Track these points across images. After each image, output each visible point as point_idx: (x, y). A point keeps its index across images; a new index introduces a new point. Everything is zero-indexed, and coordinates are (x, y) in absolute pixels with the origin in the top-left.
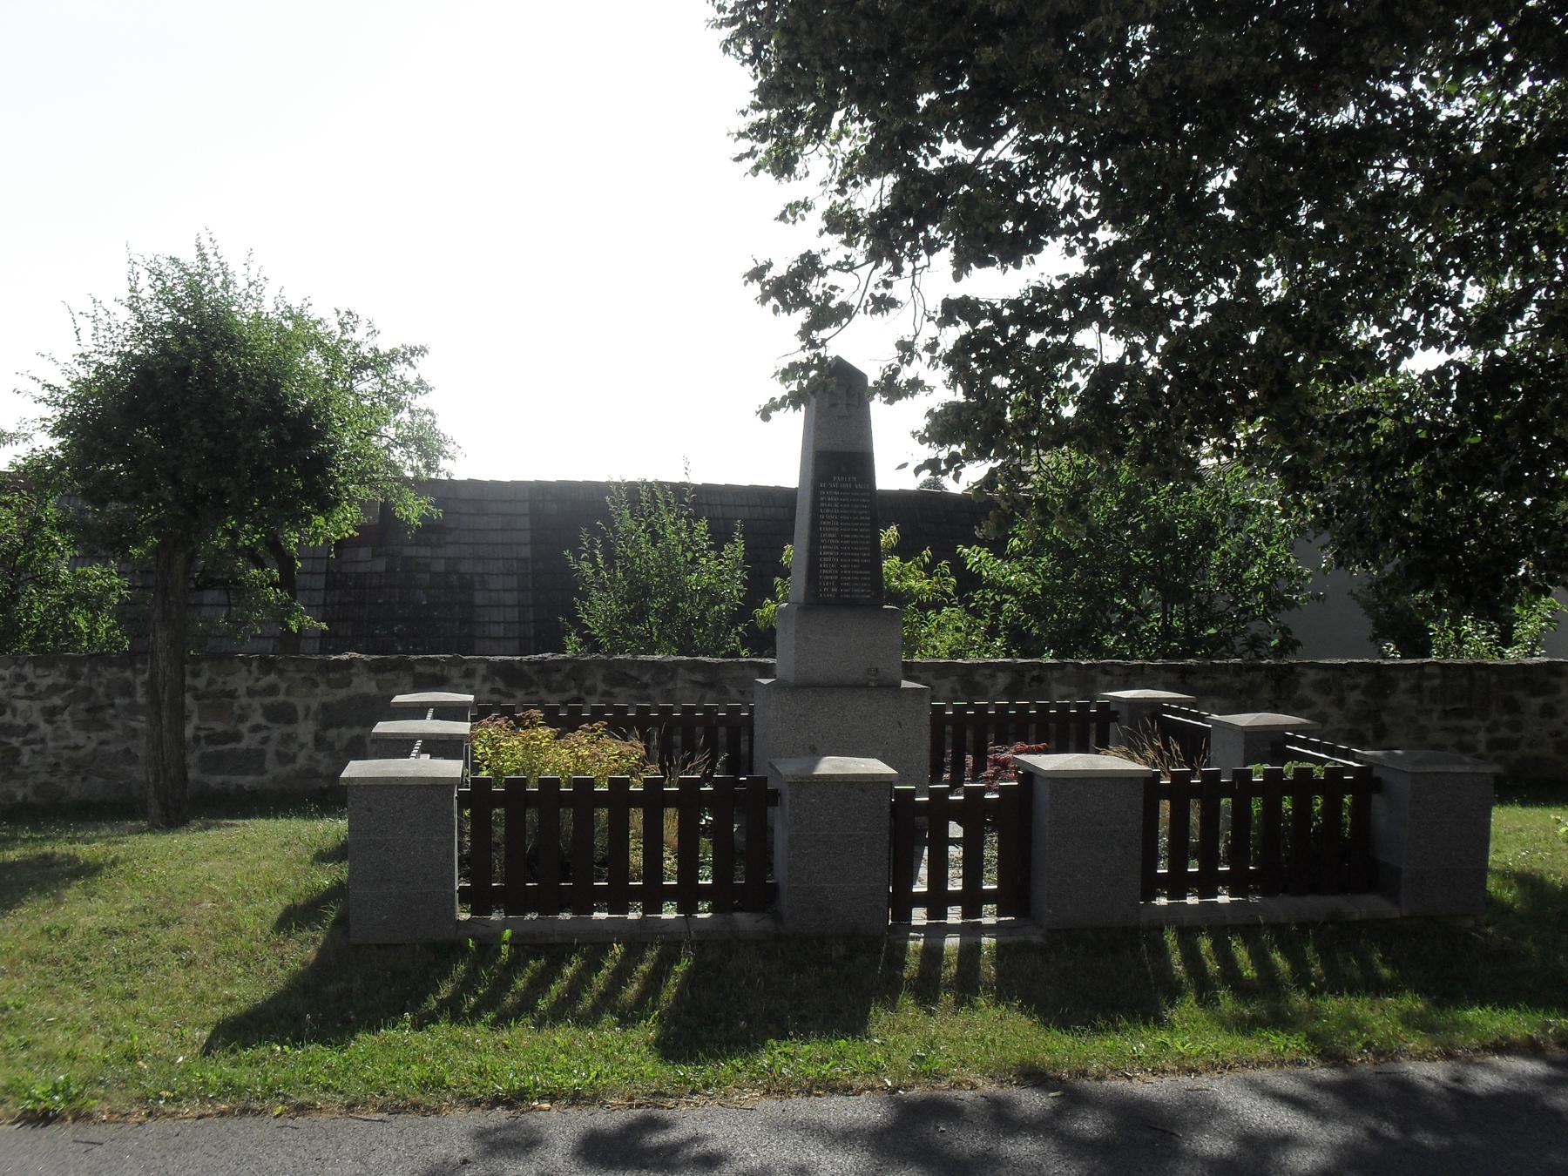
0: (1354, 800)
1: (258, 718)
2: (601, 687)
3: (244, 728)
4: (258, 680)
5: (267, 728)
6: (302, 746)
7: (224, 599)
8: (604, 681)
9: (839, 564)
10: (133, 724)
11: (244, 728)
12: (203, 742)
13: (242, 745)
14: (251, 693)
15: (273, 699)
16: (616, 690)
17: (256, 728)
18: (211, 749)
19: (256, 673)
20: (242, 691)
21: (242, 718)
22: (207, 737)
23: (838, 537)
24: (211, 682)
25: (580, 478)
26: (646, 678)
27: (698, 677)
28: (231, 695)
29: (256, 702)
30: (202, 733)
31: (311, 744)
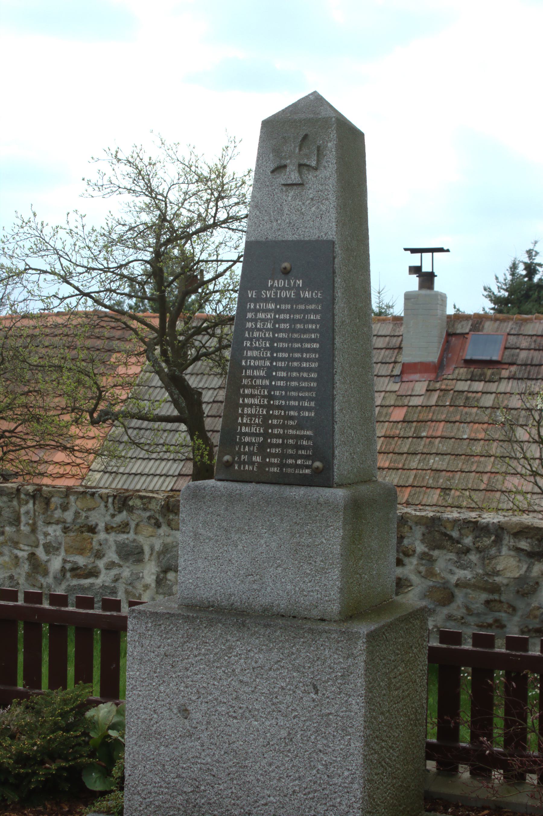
0: (463, 666)
1: (112, 555)
2: (420, 548)
3: (101, 564)
4: (113, 516)
5: (120, 566)
6: (146, 587)
7: (220, 371)
8: (423, 541)
9: (266, 418)
10: (16, 552)
11: (101, 564)
12: (68, 575)
13: (99, 581)
14: (108, 529)
15: (125, 536)
16: (436, 553)
17: (111, 566)
18: (75, 582)
19: (111, 511)
20: (101, 526)
21: (99, 555)
22: (72, 570)
23: (268, 376)
24: (77, 514)
25: (366, 144)
26: (468, 541)
27: (524, 544)
28: (92, 530)
29: (112, 538)
30: (68, 566)
31: (153, 585)
